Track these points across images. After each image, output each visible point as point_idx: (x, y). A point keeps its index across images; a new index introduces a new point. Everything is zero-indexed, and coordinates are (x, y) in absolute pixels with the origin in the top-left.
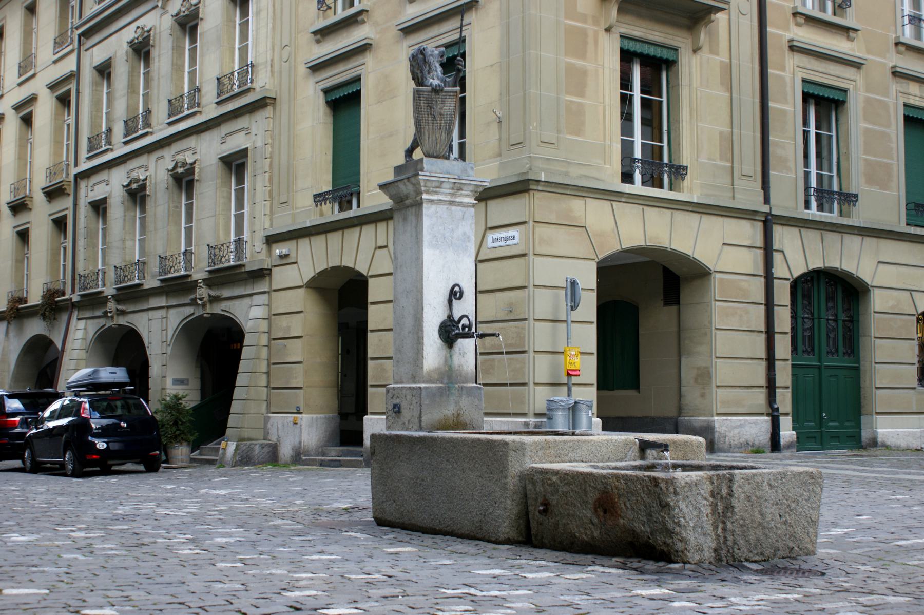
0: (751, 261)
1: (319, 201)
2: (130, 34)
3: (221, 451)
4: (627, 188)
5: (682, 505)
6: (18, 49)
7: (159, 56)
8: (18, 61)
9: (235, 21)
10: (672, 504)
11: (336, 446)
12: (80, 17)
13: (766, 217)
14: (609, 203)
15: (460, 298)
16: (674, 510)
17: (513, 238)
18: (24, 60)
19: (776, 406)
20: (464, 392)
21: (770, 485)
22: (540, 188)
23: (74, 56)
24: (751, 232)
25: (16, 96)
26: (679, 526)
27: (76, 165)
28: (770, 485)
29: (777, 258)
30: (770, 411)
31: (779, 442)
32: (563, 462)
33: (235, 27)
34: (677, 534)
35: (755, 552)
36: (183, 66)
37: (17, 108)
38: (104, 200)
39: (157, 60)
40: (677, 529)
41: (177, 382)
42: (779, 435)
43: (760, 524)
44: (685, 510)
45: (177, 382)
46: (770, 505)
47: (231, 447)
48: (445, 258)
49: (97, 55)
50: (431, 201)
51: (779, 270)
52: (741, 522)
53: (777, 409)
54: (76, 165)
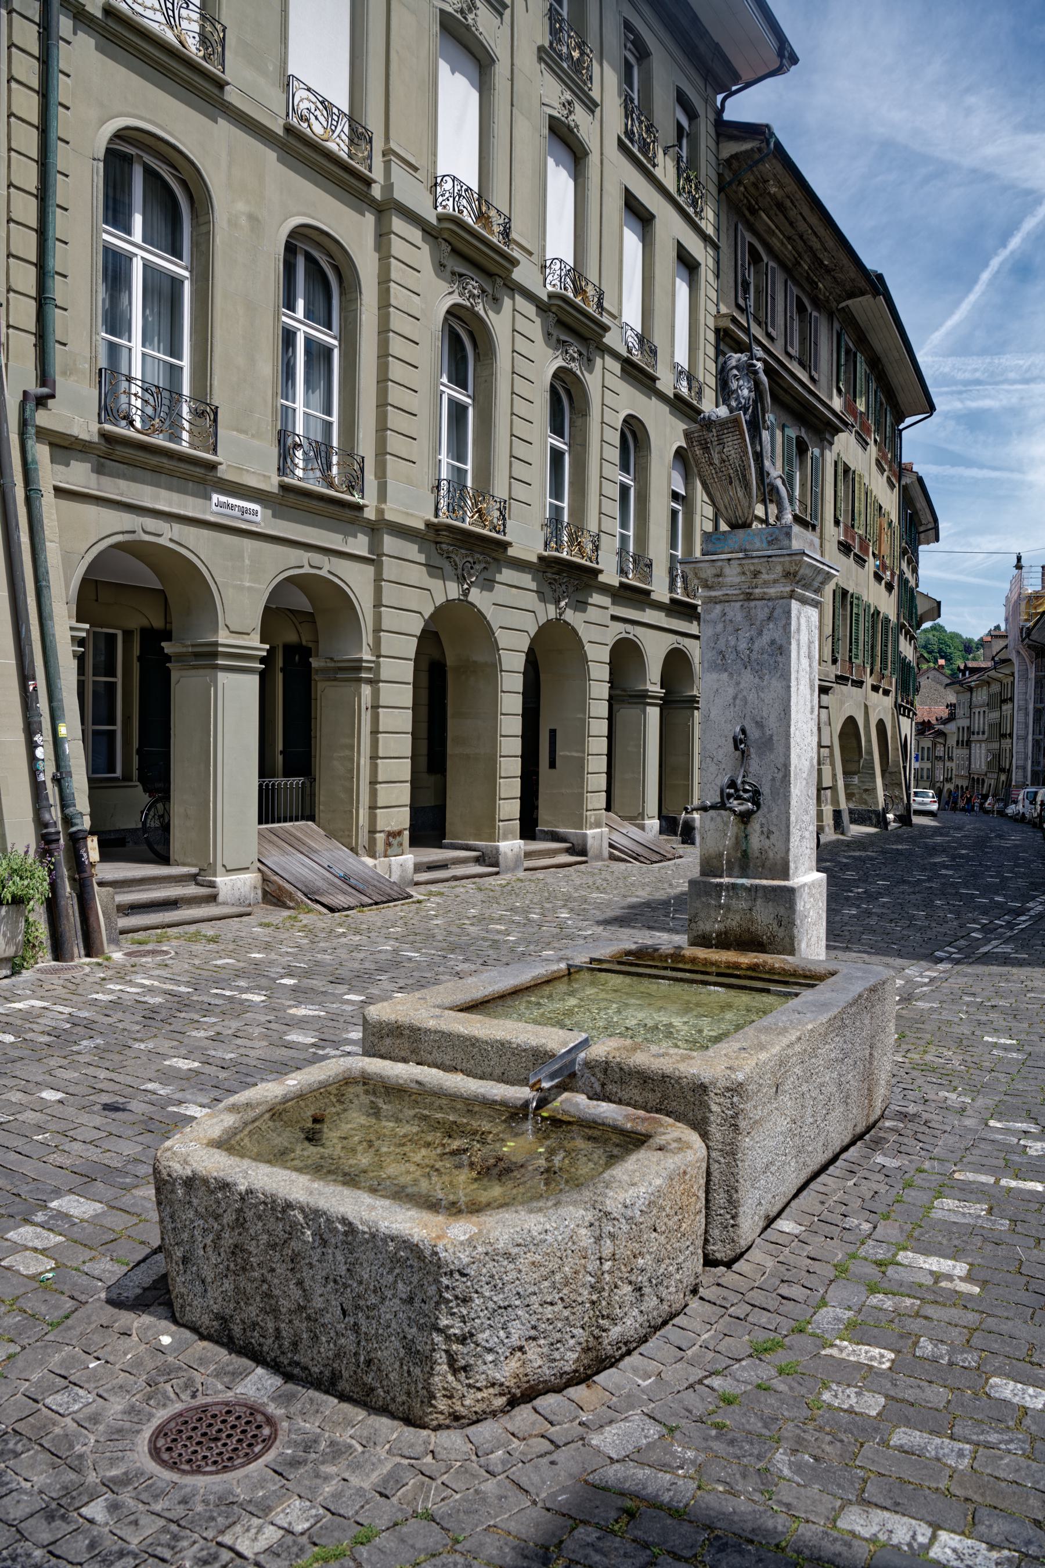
20: (760, 894)
43: (301, 1308)
48: (738, 684)
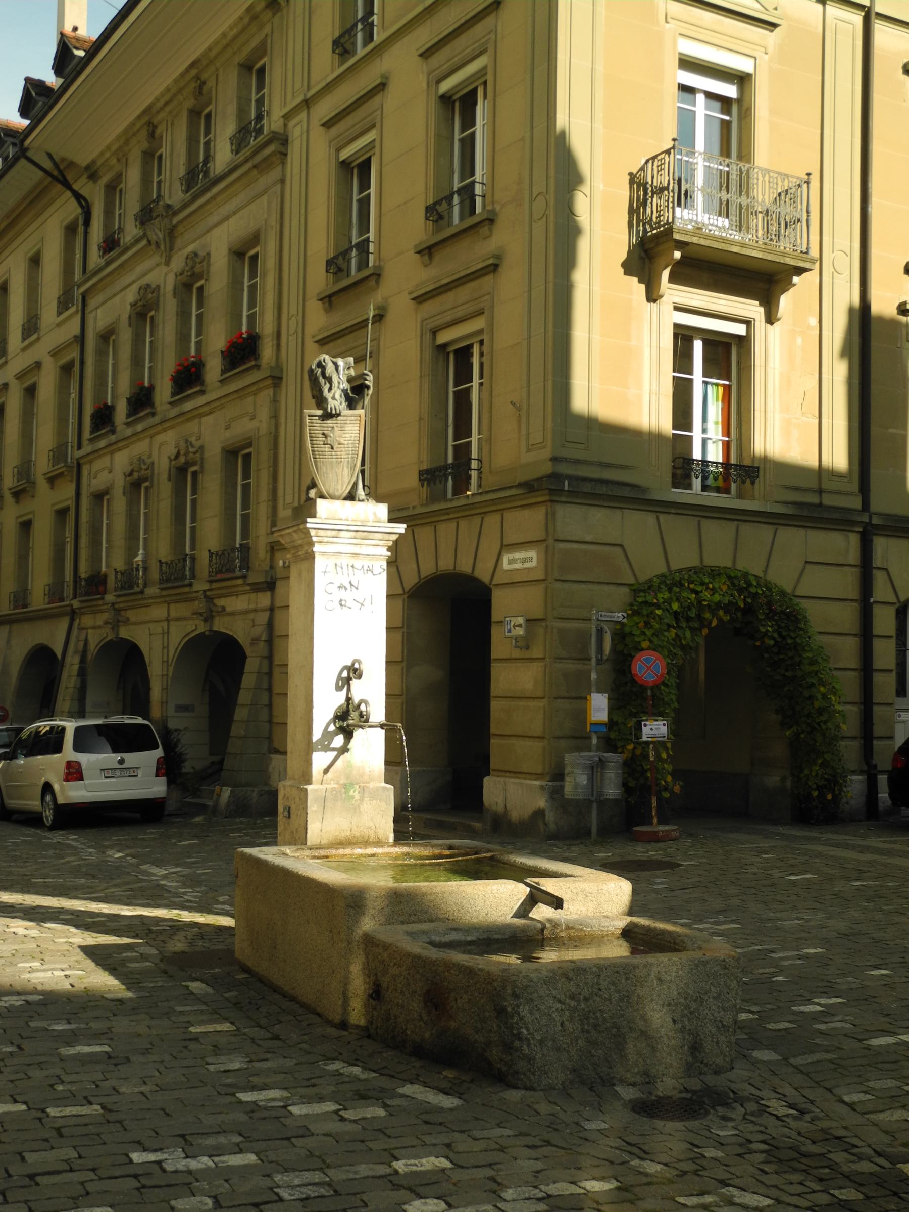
0: (845, 583)
1: (424, 480)
2: (131, 295)
3: (215, 797)
4: (679, 495)
5: (524, 1011)
6: (22, 307)
7: (163, 322)
8: (22, 323)
9: (243, 283)
10: (509, 1009)
11: (275, 826)
12: (84, 271)
13: (864, 528)
14: (654, 515)
15: (360, 677)
16: (512, 1017)
17: (531, 559)
18: (29, 321)
19: (874, 762)
21: (659, 979)
22: (563, 499)
23: (78, 318)
24: (846, 545)
25: (17, 362)
26: (520, 1039)
27: (79, 448)
28: (659, 979)
29: (879, 579)
30: (865, 768)
31: (877, 805)
32: (420, 921)
33: (243, 290)
34: (517, 1051)
35: (636, 1070)
36: (190, 336)
37: (20, 377)
38: (106, 492)
39: (160, 327)
40: (517, 1044)
41: (180, 708)
42: (876, 798)
44: (528, 1018)
45: (180, 708)
46: (657, 1007)
47: (226, 793)
49: (99, 319)
50: (323, 553)
51: (881, 591)
52: (614, 1031)
53: (875, 766)
54: (79, 448)
